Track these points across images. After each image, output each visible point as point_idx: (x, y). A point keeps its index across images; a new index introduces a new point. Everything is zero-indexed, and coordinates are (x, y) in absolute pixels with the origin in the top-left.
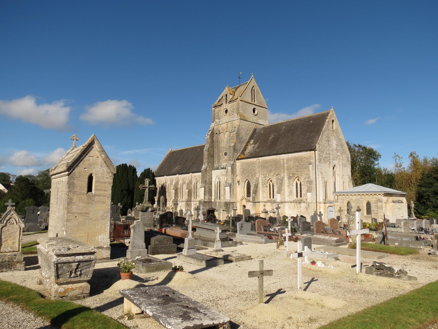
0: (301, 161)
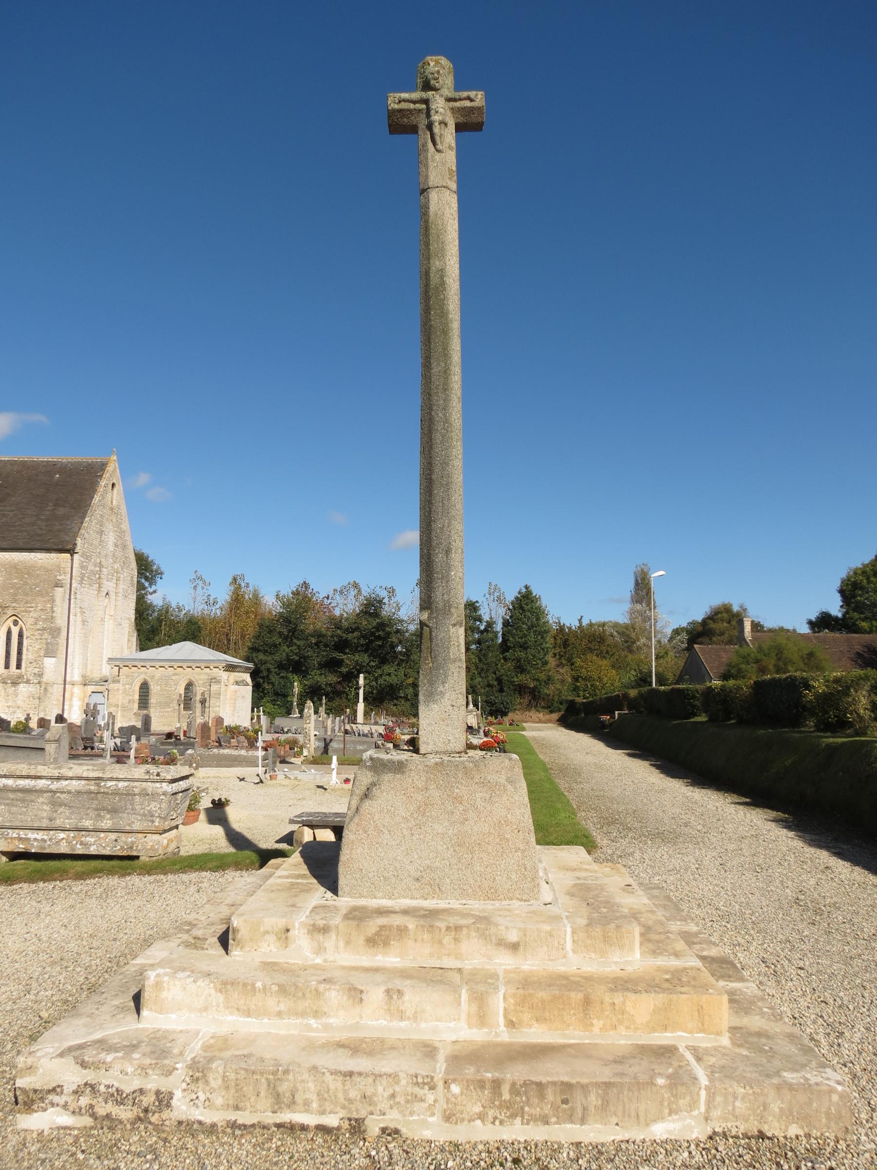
0: (28, 574)
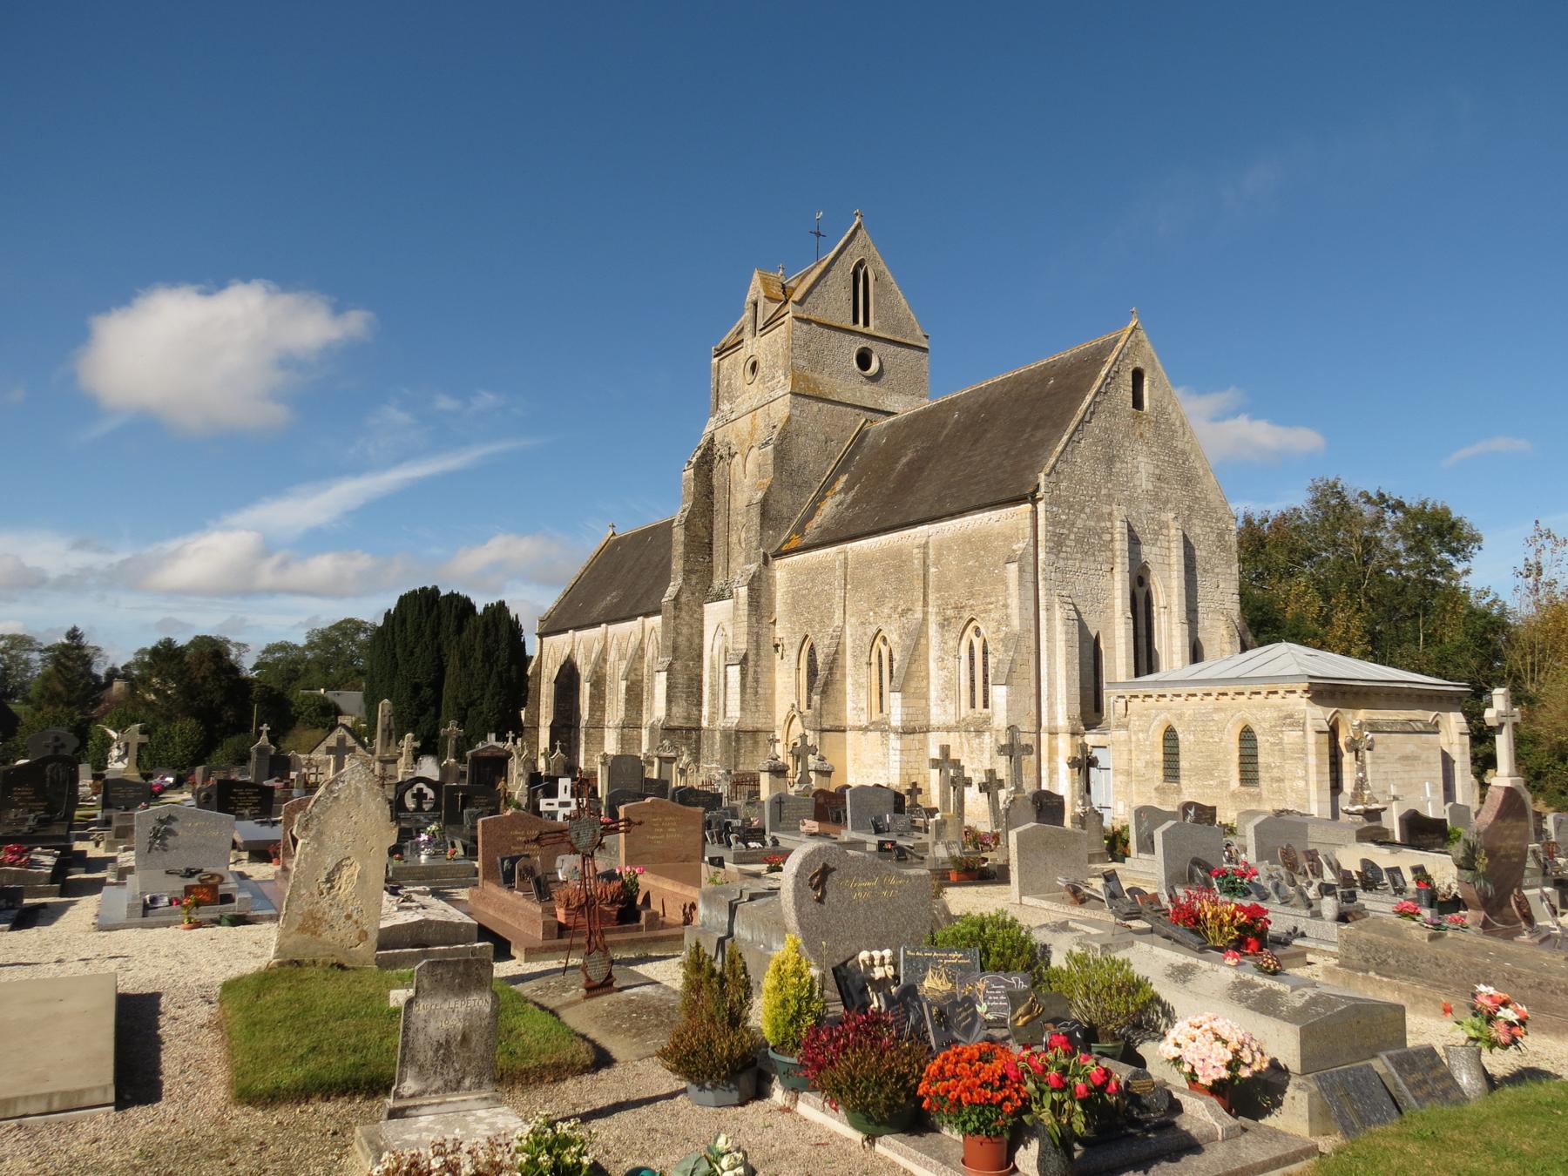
0: (984, 549)
